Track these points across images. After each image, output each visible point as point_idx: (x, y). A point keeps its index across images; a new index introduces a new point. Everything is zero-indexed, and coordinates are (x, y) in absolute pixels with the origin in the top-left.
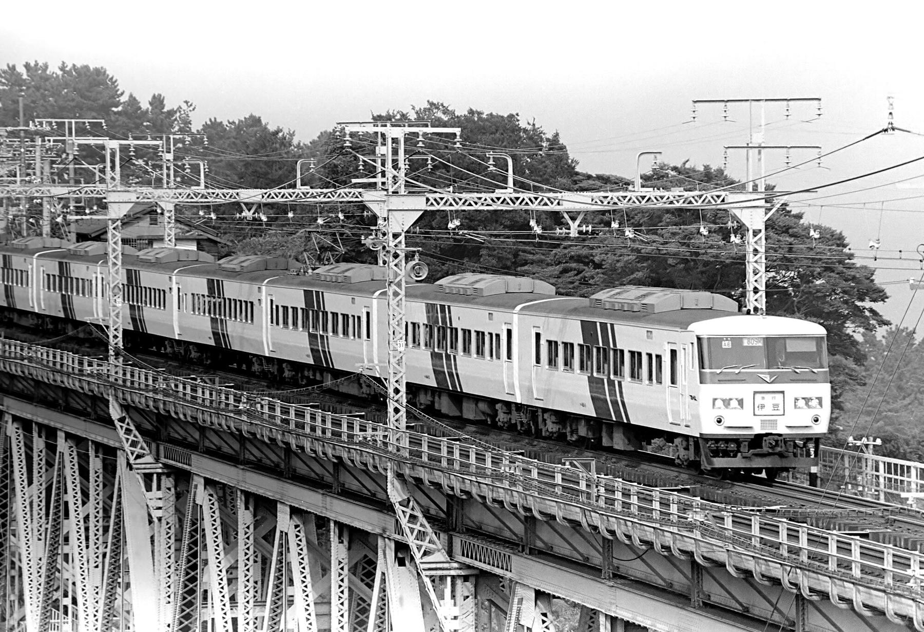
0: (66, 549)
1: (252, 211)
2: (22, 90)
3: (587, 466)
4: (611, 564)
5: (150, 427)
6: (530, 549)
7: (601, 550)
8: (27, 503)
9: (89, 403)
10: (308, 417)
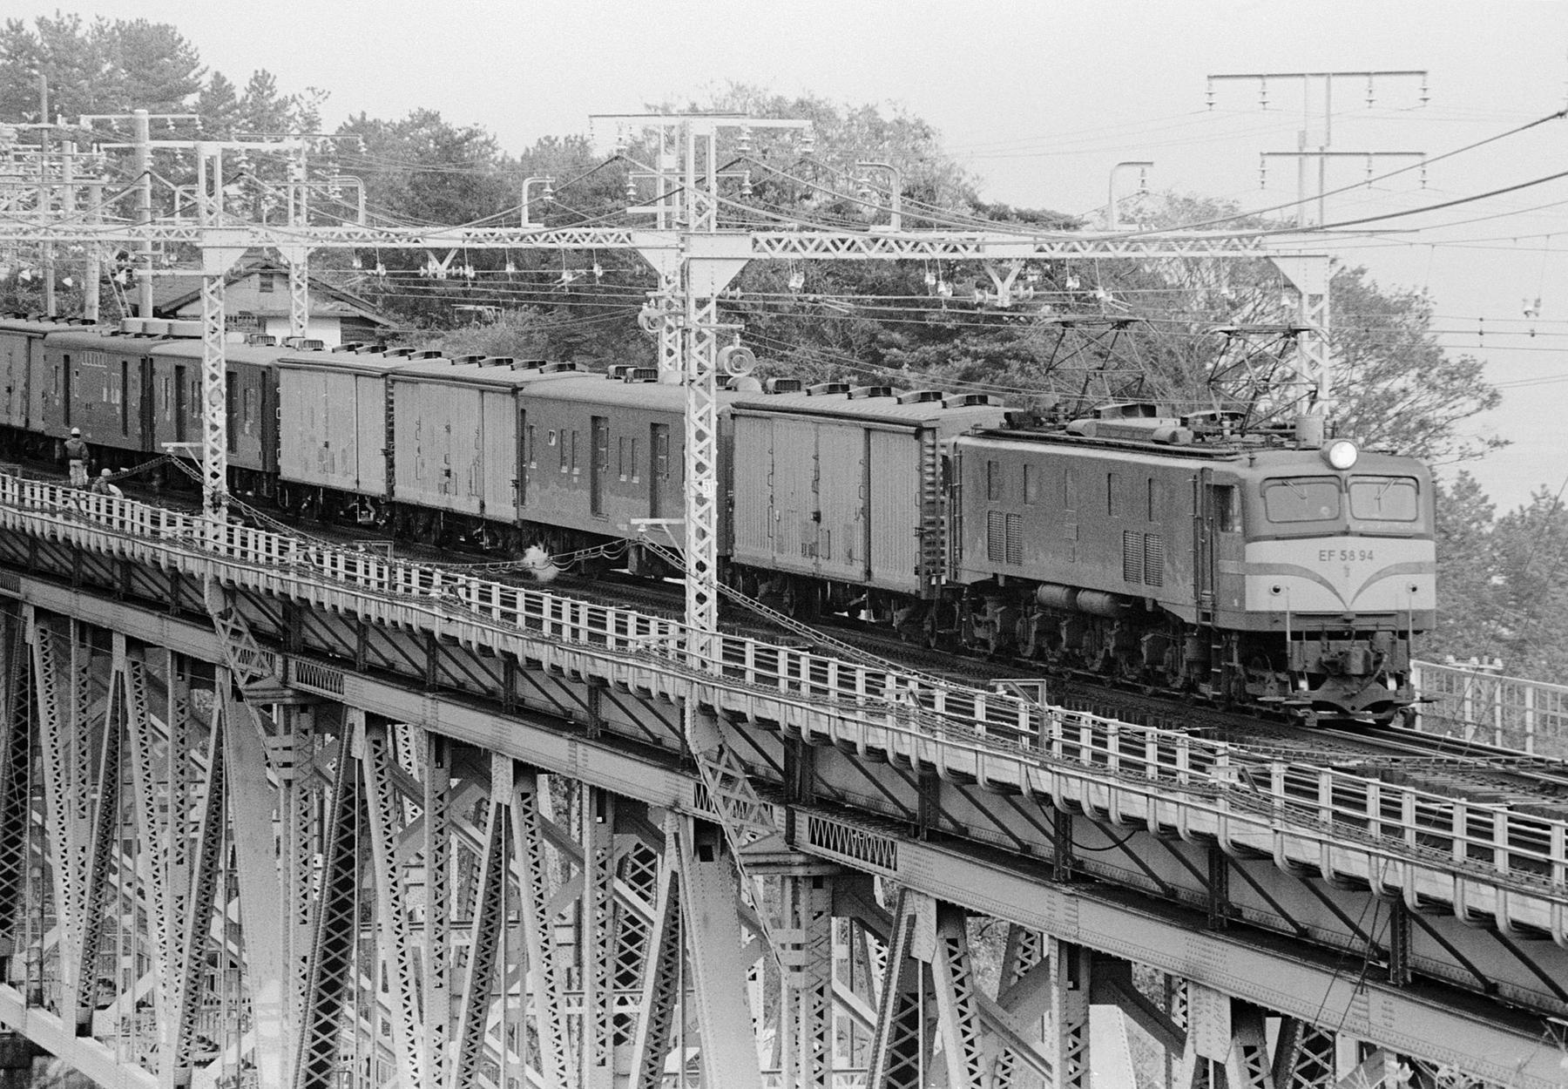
0: (128, 834)
1: (447, 262)
3: (1032, 693)
4: (1069, 855)
5: (270, 627)
7: (1052, 831)
9: (117, 573)
10: (1151, 751)
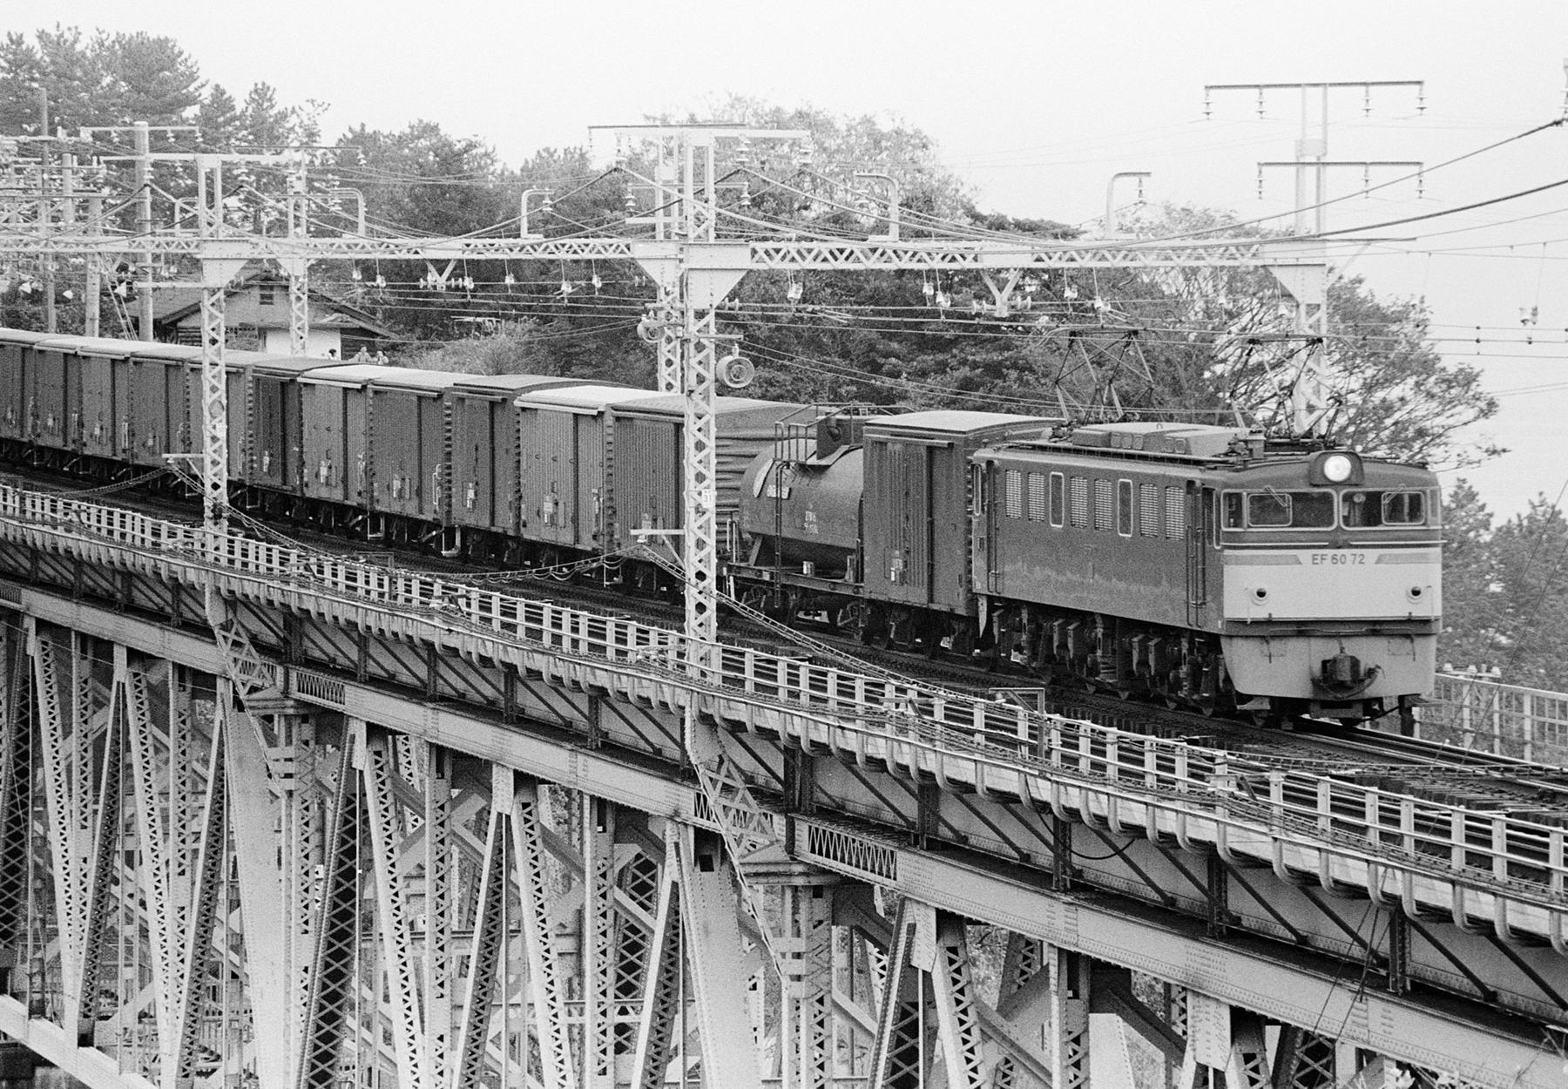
1: (446, 274)
2: (33, 79)
4: (1069, 864)
5: (273, 640)
6: (929, 840)
7: (1051, 839)
8: (62, 768)
